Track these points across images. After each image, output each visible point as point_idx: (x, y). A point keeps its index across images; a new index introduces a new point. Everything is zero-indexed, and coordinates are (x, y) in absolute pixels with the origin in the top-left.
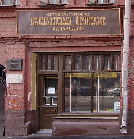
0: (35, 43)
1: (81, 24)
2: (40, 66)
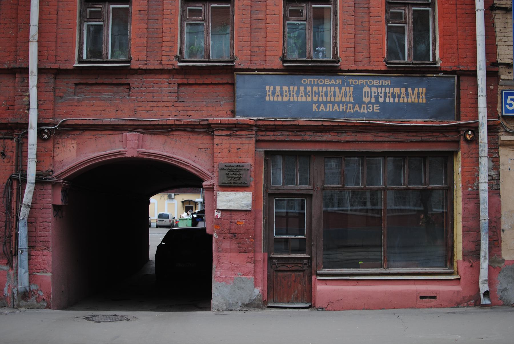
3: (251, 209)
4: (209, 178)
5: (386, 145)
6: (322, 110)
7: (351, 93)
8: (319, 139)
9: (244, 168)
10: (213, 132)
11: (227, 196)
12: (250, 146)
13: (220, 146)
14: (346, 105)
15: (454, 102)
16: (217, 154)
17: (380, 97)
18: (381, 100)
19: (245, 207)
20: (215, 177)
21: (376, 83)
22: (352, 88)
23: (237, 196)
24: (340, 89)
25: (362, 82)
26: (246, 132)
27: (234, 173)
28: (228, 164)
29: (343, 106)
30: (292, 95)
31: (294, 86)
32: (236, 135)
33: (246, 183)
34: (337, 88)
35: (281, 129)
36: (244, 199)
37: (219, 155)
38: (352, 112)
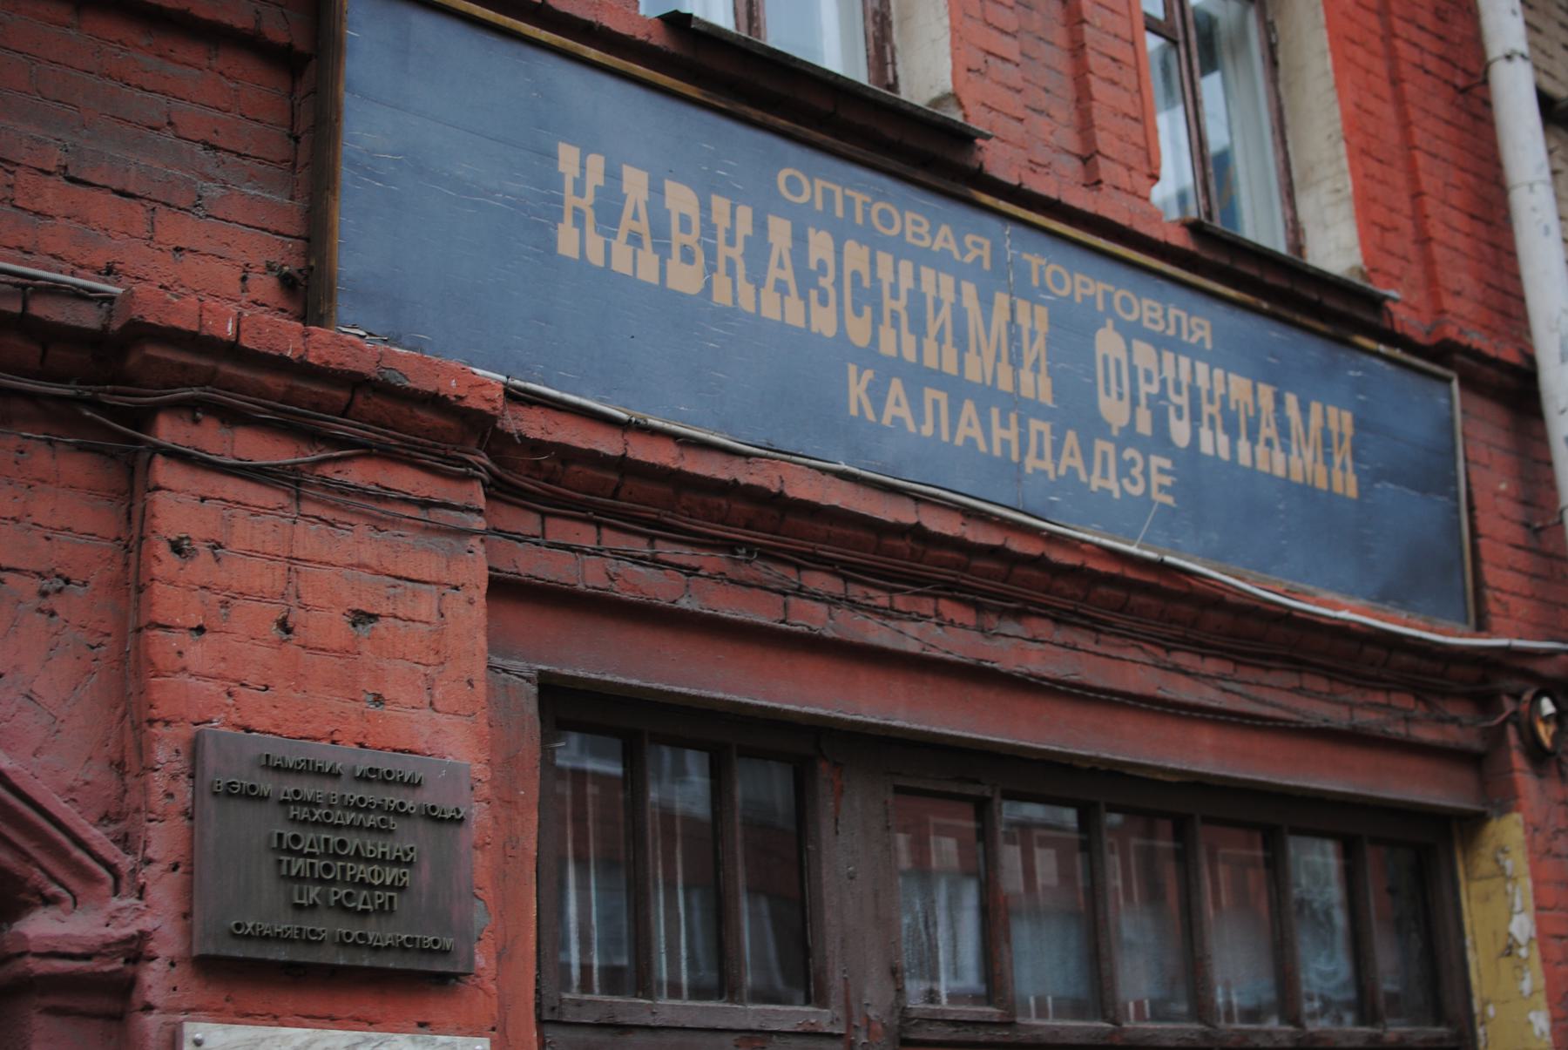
0: (561, 530)
1: (1144, 426)
2: (1145, 1020)
4: (89, 878)
5: (1206, 736)
6: (897, 420)
7: (1040, 343)
8: (878, 634)
9: (425, 797)
10: (143, 419)
12: (456, 601)
13: (201, 567)
14: (1022, 423)
15: (1459, 523)
16: (175, 640)
17: (1172, 412)
18: (1180, 432)
20: (155, 869)
22: (1042, 312)
24: (986, 302)
25: (1089, 292)
26: (424, 478)
27: (342, 844)
28: (292, 754)
29: (1005, 424)
30: (722, 265)
31: (736, 198)
32: (345, 490)
33: (448, 942)
34: (969, 289)
35: (652, 513)
37: (197, 653)
38: (1052, 476)
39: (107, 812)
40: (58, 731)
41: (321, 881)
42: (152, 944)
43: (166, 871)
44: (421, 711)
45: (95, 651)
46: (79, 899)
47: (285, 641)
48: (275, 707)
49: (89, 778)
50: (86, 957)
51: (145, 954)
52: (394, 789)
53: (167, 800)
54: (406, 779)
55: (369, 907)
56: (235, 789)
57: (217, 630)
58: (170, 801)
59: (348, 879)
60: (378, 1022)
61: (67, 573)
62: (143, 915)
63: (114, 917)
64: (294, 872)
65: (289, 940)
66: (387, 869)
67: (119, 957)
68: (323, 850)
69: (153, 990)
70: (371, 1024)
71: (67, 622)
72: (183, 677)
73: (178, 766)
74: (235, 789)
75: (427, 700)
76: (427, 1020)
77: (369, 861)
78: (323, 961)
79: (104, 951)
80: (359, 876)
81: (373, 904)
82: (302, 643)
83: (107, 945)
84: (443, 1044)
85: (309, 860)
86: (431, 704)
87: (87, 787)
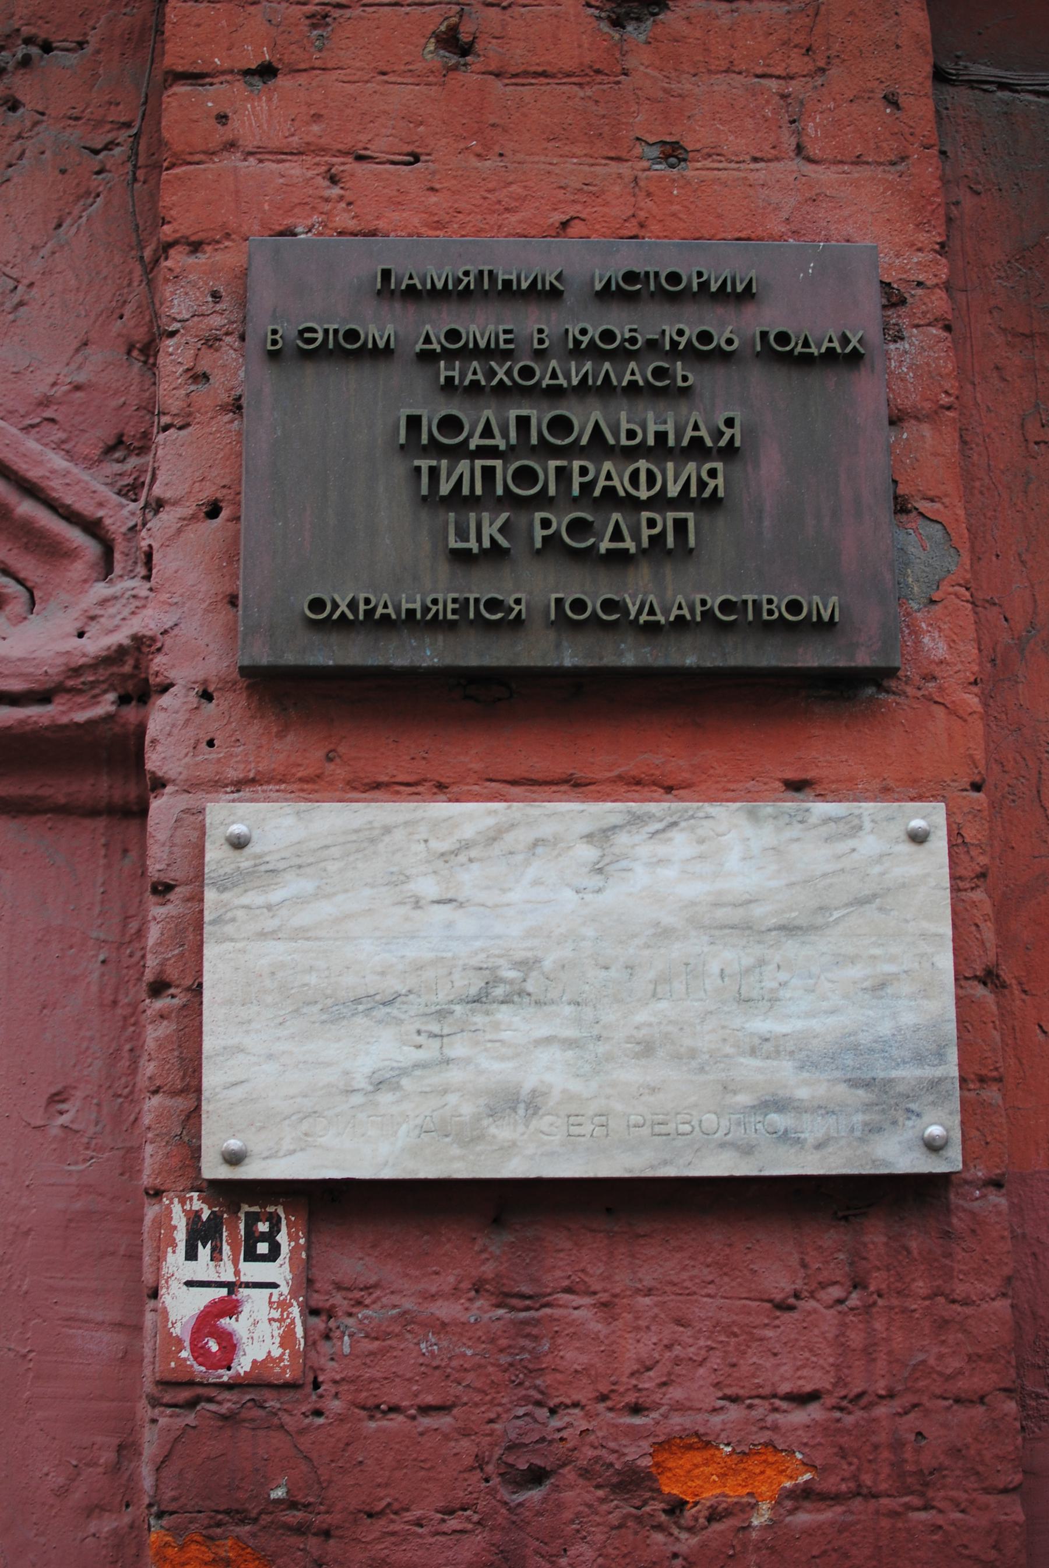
3: (951, 1162)
11: (427, 887)
19: (813, 1128)
20: (168, 517)
21: (643, 477)
23: (641, 877)
27: (559, 425)
36: (791, 948)
39: (121, 435)
40: (21, 304)
41: (510, 500)
42: (159, 659)
43: (193, 517)
44: (772, 165)
45: (101, 156)
46: (38, 594)
47: (455, 68)
48: (432, 189)
49: (81, 378)
50: (44, 697)
51: (152, 680)
52: (690, 310)
53: (193, 388)
54: (714, 288)
55: (629, 545)
56: (313, 340)
57: (303, 66)
58: (202, 388)
59: (576, 491)
60: (686, 785)
61: (42, 32)
62: (144, 606)
63: (93, 618)
64: (445, 489)
65: (436, 624)
66: (670, 466)
67: (105, 692)
68: (513, 441)
69: (159, 748)
70: (669, 789)
71: (43, 114)
72: (233, 160)
73: (217, 321)
74: (313, 340)
75: (789, 142)
76: (808, 776)
77: (630, 453)
78: (524, 661)
79: (70, 683)
80: (602, 483)
81: (636, 537)
82: (493, 67)
83: (76, 671)
84: (828, 820)
85: (479, 463)
86: (799, 149)
87: (79, 394)
